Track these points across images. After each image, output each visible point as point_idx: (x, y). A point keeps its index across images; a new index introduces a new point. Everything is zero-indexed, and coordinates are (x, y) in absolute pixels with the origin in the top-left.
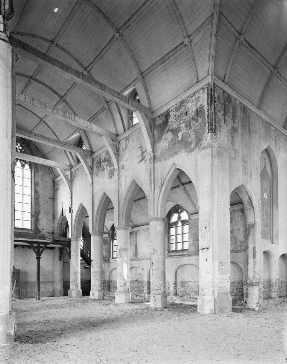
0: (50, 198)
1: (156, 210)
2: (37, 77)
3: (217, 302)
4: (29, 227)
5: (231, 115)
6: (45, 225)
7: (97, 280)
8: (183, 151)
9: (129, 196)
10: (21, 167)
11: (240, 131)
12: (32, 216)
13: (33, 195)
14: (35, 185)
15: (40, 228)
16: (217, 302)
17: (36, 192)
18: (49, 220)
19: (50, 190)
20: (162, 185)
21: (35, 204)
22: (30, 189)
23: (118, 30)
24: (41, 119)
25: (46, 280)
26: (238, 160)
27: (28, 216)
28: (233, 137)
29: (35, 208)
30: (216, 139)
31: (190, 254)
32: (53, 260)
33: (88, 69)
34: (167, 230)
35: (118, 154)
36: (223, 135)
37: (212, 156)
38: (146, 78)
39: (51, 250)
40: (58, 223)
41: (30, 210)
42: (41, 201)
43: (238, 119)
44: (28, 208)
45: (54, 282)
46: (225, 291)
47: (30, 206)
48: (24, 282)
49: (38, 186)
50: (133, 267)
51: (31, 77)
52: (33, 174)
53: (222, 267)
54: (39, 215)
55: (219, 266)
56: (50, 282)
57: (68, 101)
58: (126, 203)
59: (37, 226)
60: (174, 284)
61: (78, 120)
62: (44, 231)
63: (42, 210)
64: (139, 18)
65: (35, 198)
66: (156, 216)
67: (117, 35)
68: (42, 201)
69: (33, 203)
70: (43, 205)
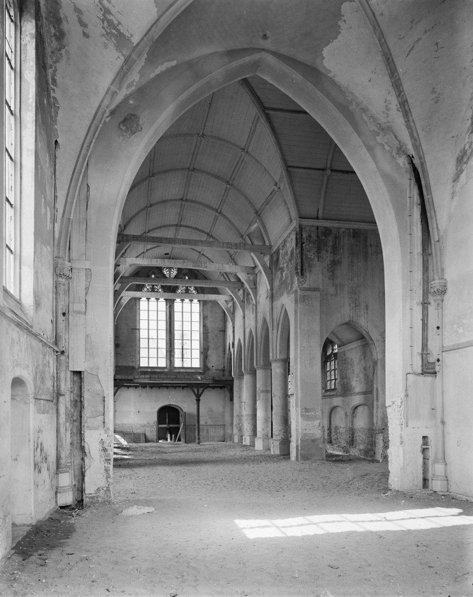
0: (220, 331)
1: (275, 351)
2: (182, 224)
3: (300, 448)
4: (198, 366)
5: (329, 249)
6: (215, 362)
7: (249, 423)
8: (285, 294)
9: (264, 333)
10: (190, 302)
11: (345, 261)
12: (201, 353)
13: (202, 329)
14: (204, 319)
15: (210, 365)
16: (300, 448)
17: (205, 326)
18: (219, 357)
19: (220, 322)
20: (278, 325)
21: (204, 340)
22: (199, 323)
23: (228, 182)
24: (200, 252)
25: (216, 423)
26: (342, 295)
27: (197, 354)
28: (333, 272)
29: (204, 344)
30: (304, 281)
31: (338, 394)
32: (224, 400)
33: (219, 211)
34: (324, 364)
35: (256, 288)
36: (317, 276)
37: (296, 301)
38: (261, 215)
39: (221, 389)
40: (228, 358)
41: (198, 347)
42: (210, 336)
43: (343, 248)
44: (196, 345)
45: (224, 425)
46: (312, 438)
47: (198, 342)
48: (192, 425)
49: (207, 320)
50: (356, 408)
51: (177, 225)
52: (202, 306)
53: (307, 414)
54: (208, 351)
55: (302, 412)
56: (221, 425)
57: (215, 236)
58: (263, 341)
59: (206, 363)
60: (328, 429)
61: (208, 265)
62: (214, 368)
63: (211, 346)
64: (239, 172)
65: (204, 333)
66: (275, 357)
67: (228, 186)
68: (211, 336)
69: (202, 339)
70: (213, 339)
